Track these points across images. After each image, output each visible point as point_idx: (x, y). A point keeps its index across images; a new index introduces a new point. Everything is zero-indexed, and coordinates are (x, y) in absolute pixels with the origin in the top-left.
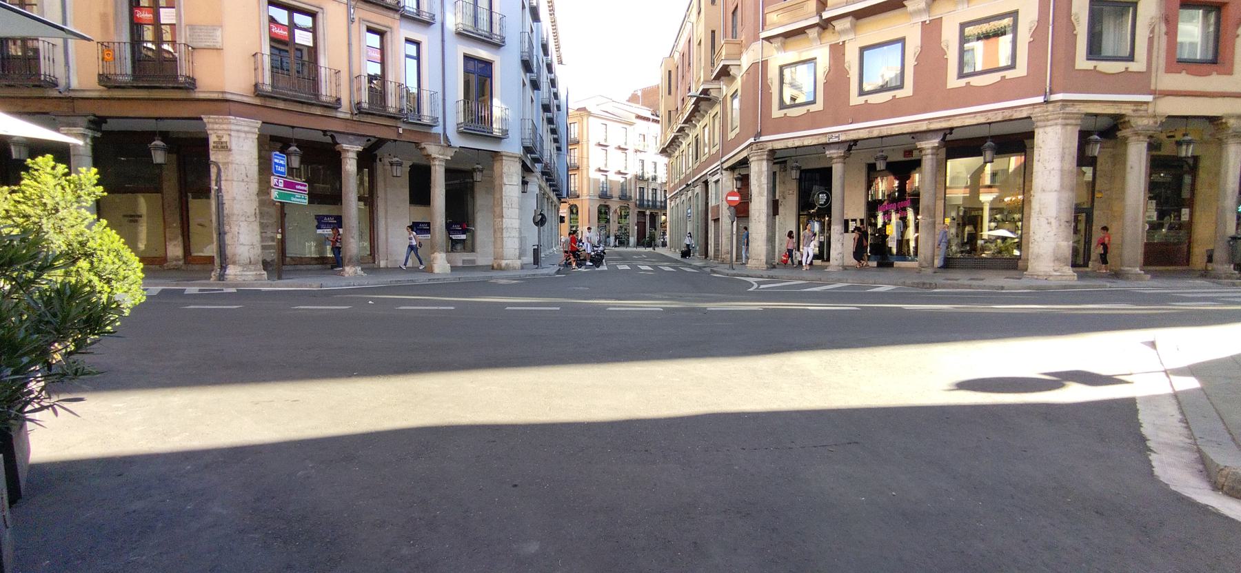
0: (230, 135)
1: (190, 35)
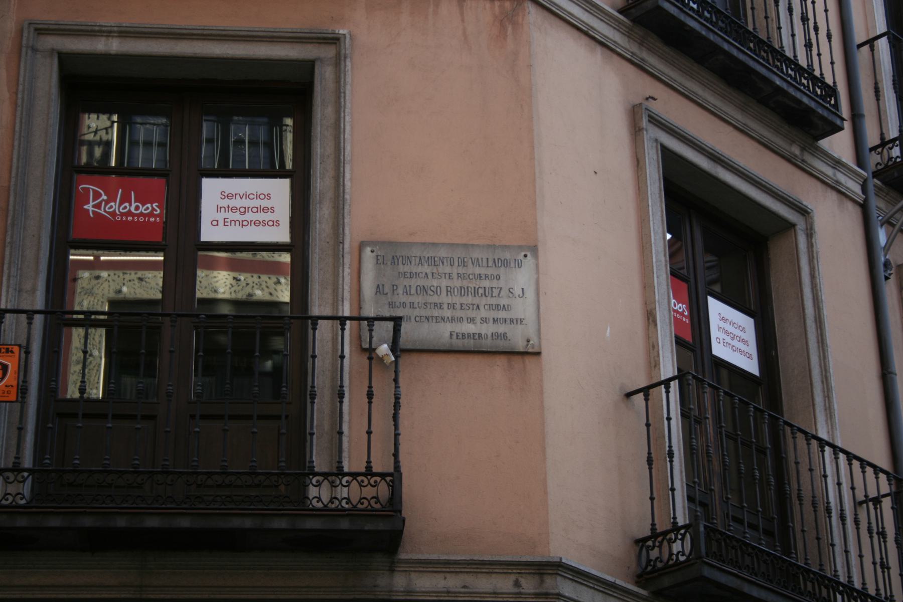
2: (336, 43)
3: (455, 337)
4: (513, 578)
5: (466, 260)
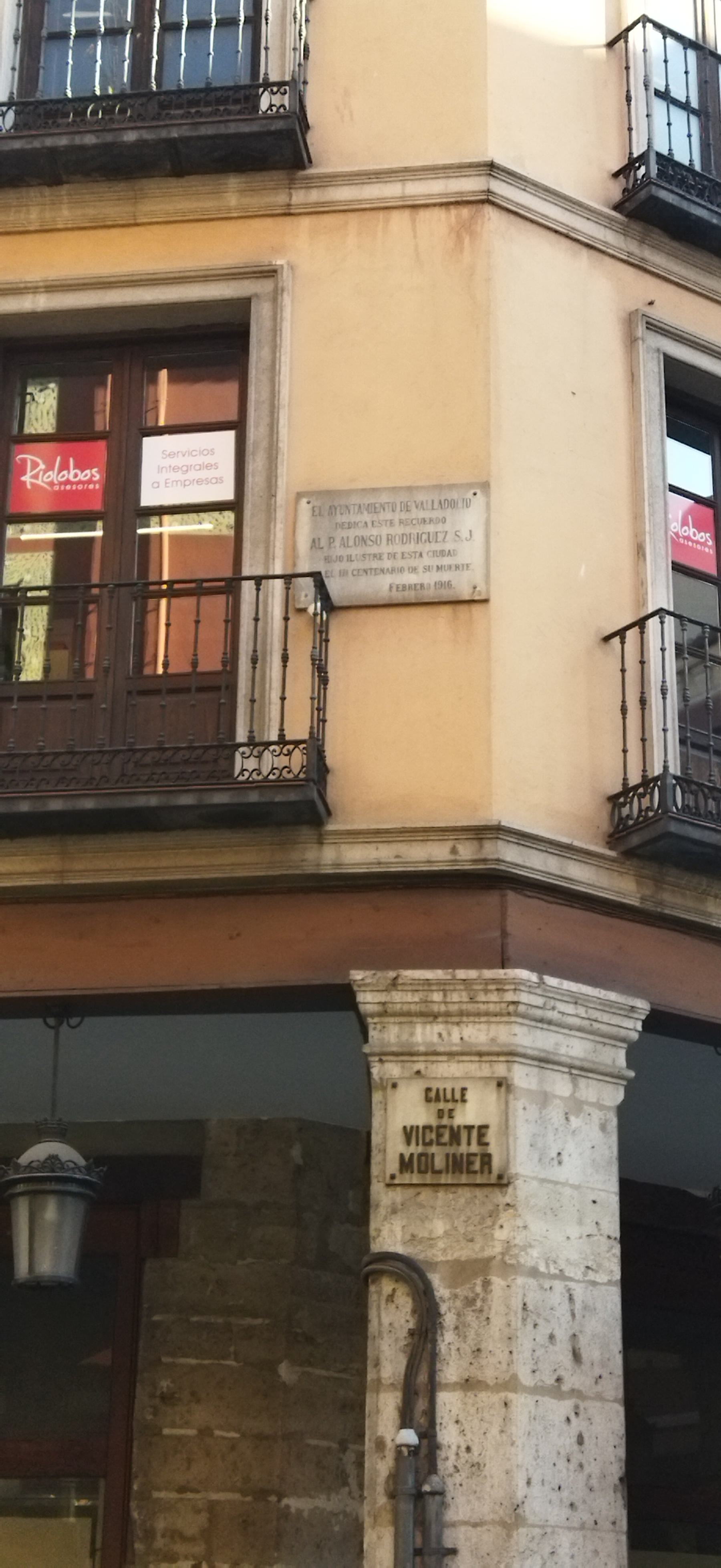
0: (502, 1084)
1: (315, 544)
2: (273, 276)
3: (394, 589)
4: (450, 844)
5: (409, 504)
